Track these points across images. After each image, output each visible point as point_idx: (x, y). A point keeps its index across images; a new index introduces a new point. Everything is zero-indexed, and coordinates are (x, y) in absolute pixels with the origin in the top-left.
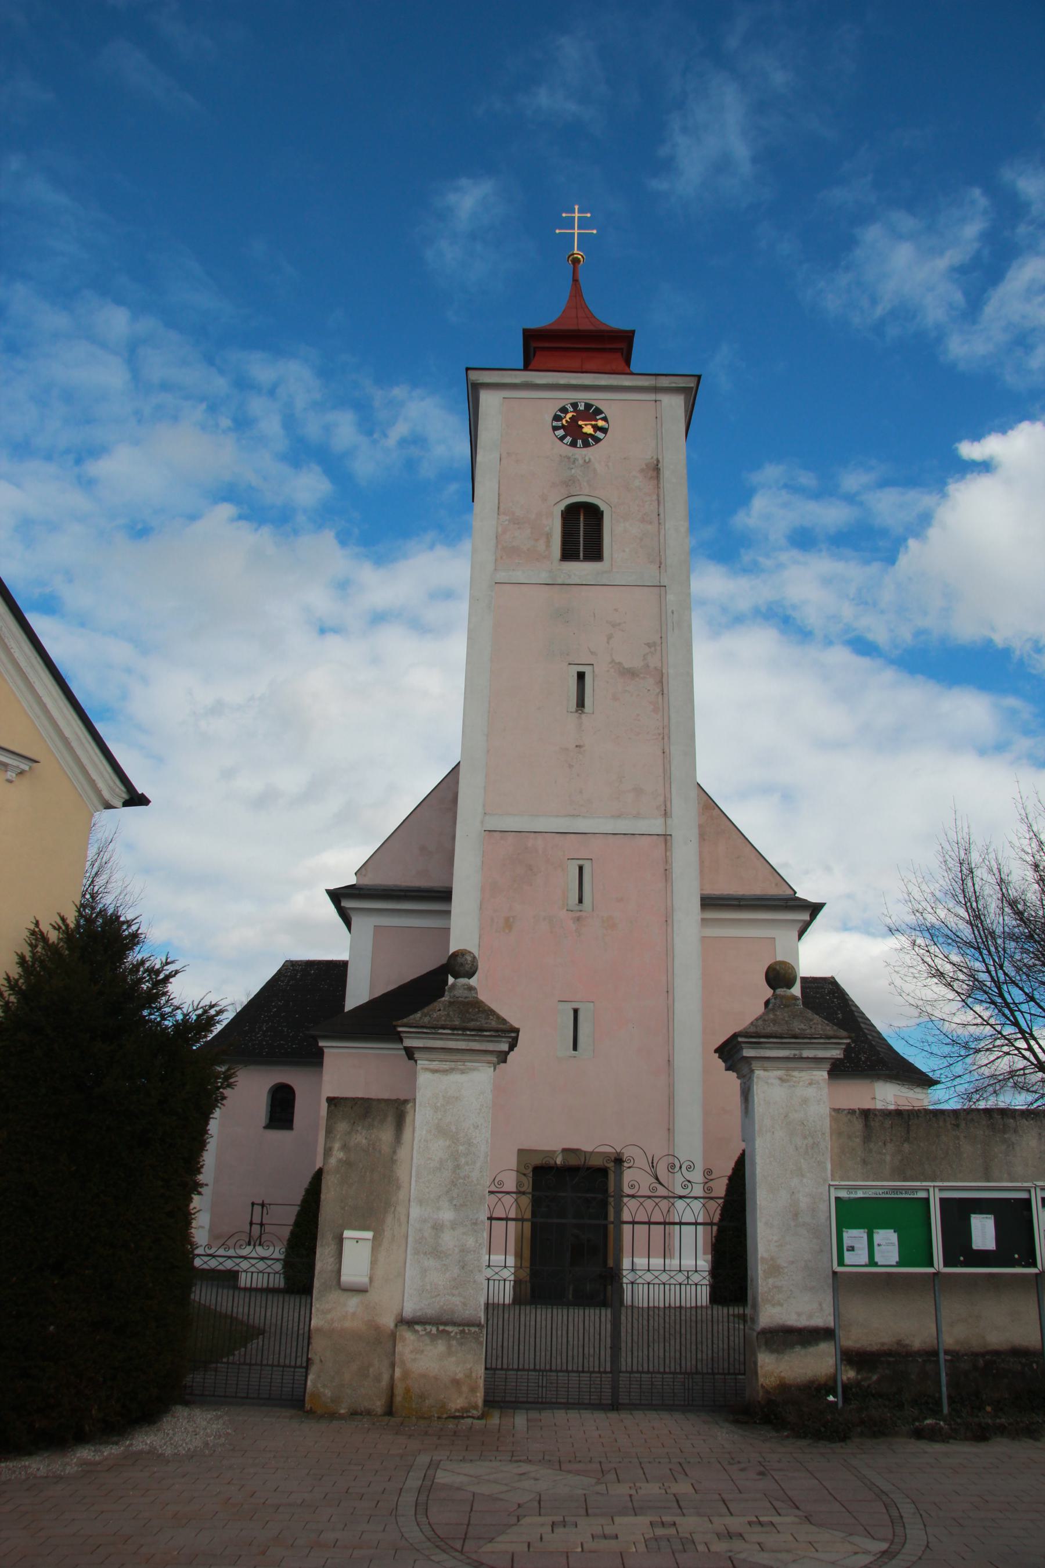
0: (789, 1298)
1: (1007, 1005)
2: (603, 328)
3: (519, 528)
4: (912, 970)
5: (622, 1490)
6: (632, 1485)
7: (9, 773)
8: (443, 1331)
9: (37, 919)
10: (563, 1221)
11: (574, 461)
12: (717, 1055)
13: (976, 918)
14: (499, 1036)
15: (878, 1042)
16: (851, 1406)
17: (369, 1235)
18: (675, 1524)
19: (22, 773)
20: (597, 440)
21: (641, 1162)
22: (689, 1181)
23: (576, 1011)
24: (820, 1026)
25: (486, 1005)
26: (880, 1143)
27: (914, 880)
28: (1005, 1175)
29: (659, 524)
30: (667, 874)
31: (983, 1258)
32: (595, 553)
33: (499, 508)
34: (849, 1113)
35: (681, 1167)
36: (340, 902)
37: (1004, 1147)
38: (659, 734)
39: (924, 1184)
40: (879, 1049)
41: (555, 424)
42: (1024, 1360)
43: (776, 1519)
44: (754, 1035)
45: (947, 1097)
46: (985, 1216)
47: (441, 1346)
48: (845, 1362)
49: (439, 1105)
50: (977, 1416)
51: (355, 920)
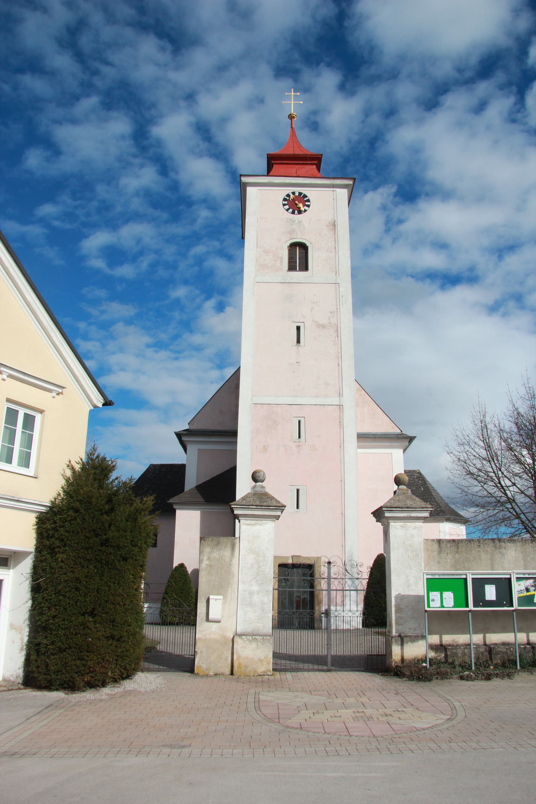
0: (405, 622)
1: (502, 487)
2: (307, 153)
3: (267, 255)
4: (458, 472)
5: (339, 701)
6: (343, 699)
7: (53, 393)
8: (255, 638)
9: (70, 459)
10: (311, 590)
11: (294, 221)
12: (372, 515)
13: (488, 447)
14: (277, 509)
15: (440, 502)
16: (433, 667)
17: (221, 597)
18: (363, 712)
19: (58, 394)
20: (305, 211)
21: (340, 563)
22: (361, 572)
23: (298, 491)
24: (419, 503)
25: (270, 495)
26: (445, 554)
27: (459, 429)
28: (500, 568)
29: (336, 252)
30: (341, 423)
31: (490, 603)
32: (305, 267)
33: (257, 245)
34: (432, 541)
35: (357, 566)
36: (181, 438)
37: (500, 555)
38: (336, 356)
39: (465, 572)
40: (441, 505)
41: (284, 202)
42: (507, 647)
43: (404, 709)
44: (390, 507)
45: (474, 531)
46: (491, 585)
47: (254, 645)
48: (430, 649)
49: (250, 539)
50: (487, 670)
51: (189, 447)
